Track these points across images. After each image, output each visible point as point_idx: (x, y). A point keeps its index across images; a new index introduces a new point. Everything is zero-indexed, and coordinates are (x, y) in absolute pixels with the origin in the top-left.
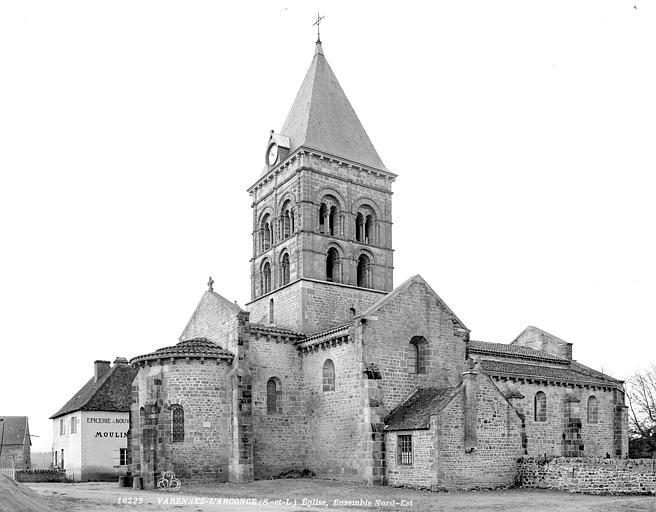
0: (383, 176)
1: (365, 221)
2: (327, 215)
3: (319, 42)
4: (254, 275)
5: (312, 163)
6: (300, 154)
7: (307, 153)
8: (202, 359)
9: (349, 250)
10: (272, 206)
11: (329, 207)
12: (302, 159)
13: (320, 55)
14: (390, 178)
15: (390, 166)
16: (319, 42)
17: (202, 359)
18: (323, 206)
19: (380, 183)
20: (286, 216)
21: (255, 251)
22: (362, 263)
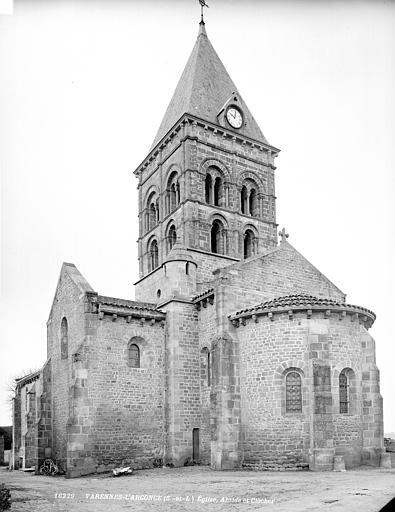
0: (266, 151)
1: (214, 184)
2: (213, 187)
3: (202, 23)
4: (141, 257)
5: (196, 132)
6: (184, 123)
7: (191, 122)
8: (310, 312)
9: (236, 221)
10: (159, 181)
11: (214, 177)
12: (186, 128)
13: (203, 35)
14: (273, 153)
15: (272, 140)
16: (202, 23)
17: (310, 312)
18: (209, 177)
19: (264, 158)
20: (173, 189)
21: (141, 231)
22: (248, 238)
